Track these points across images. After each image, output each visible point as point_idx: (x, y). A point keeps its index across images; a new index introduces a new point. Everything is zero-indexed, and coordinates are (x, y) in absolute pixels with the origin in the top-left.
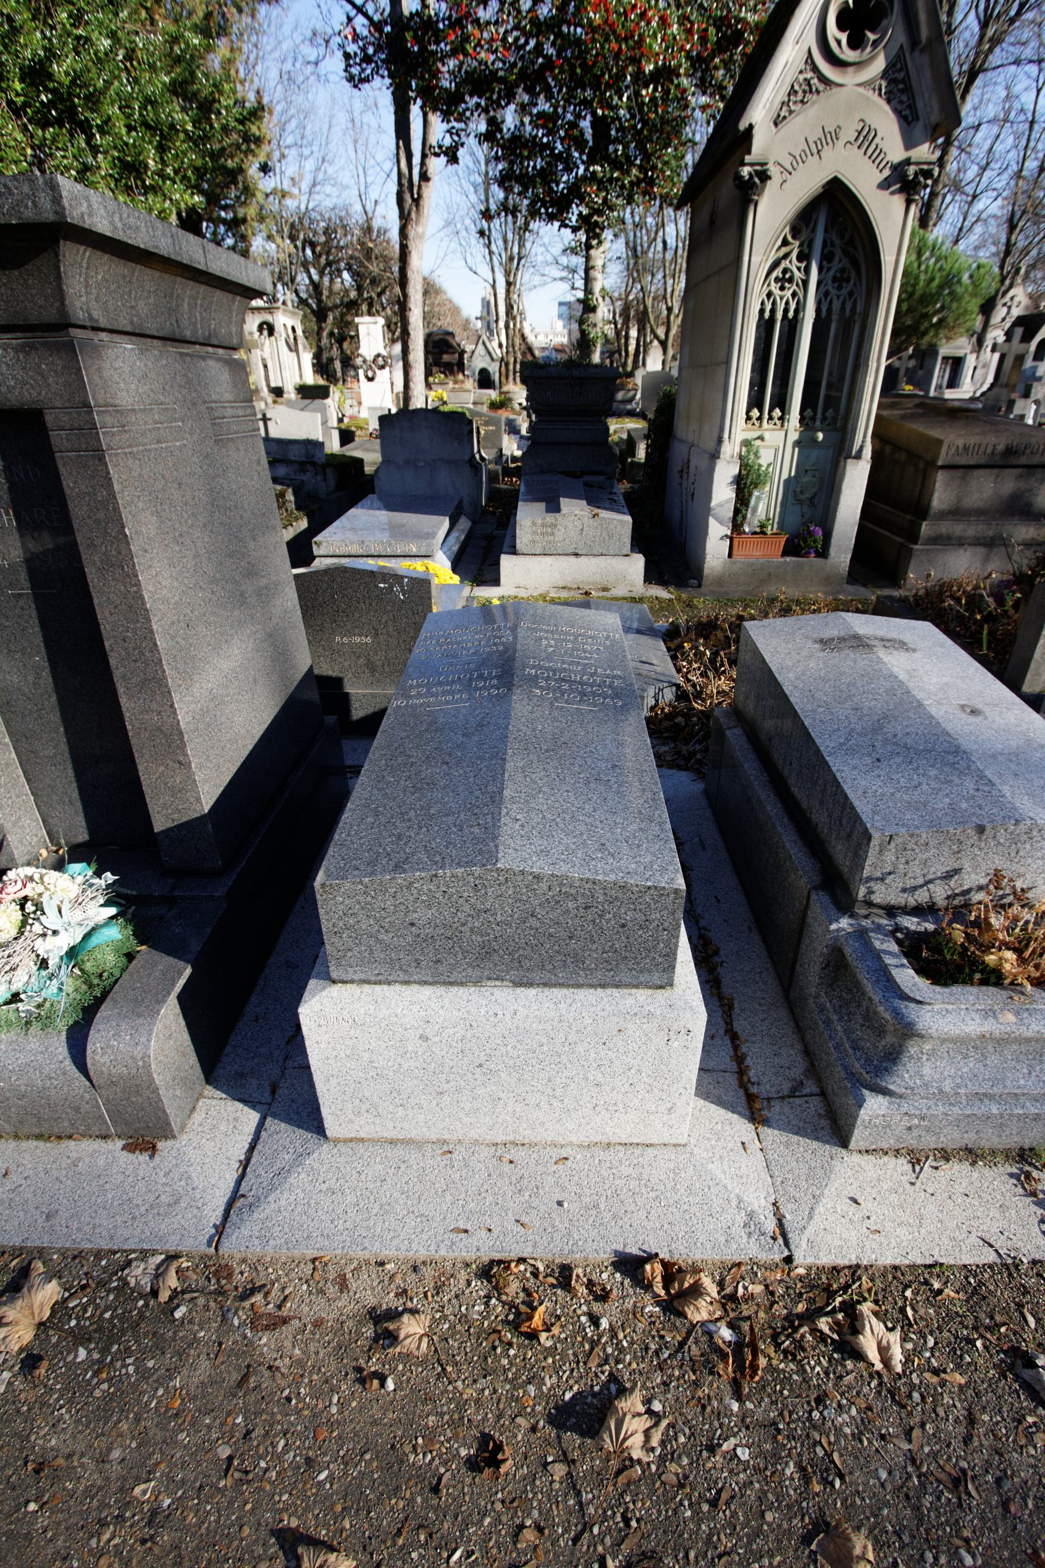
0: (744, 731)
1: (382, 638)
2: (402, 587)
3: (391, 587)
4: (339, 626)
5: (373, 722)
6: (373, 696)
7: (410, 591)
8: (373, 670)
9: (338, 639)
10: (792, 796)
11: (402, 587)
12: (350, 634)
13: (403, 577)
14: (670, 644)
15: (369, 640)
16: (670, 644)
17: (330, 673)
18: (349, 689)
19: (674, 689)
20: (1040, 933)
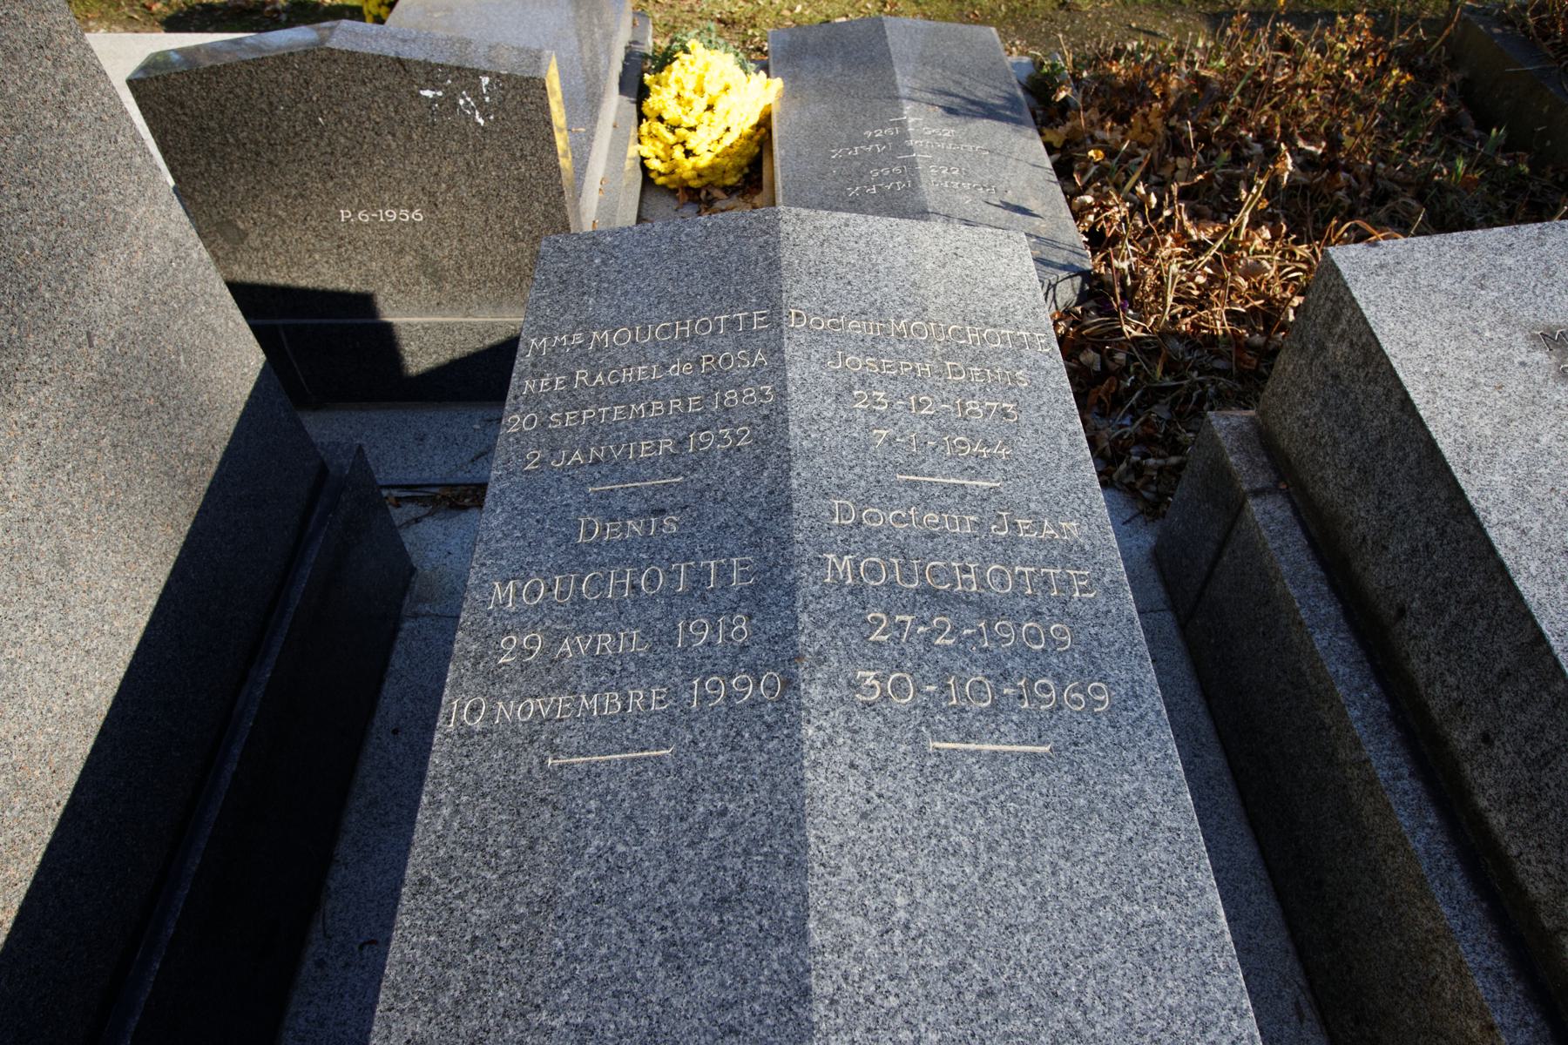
0: (1296, 511)
1: (447, 212)
2: (478, 96)
3: (451, 98)
4: (342, 186)
5: (483, 376)
6: (447, 329)
7: (500, 106)
8: (437, 277)
9: (344, 214)
10: (1478, 820)
11: (478, 96)
12: (371, 202)
13: (477, 74)
14: (1051, 136)
15: (418, 215)
16: (1050, 136)
17: (342, 285)
18: (391, 314)
19: (1078, 280)
20: (726, 4)
